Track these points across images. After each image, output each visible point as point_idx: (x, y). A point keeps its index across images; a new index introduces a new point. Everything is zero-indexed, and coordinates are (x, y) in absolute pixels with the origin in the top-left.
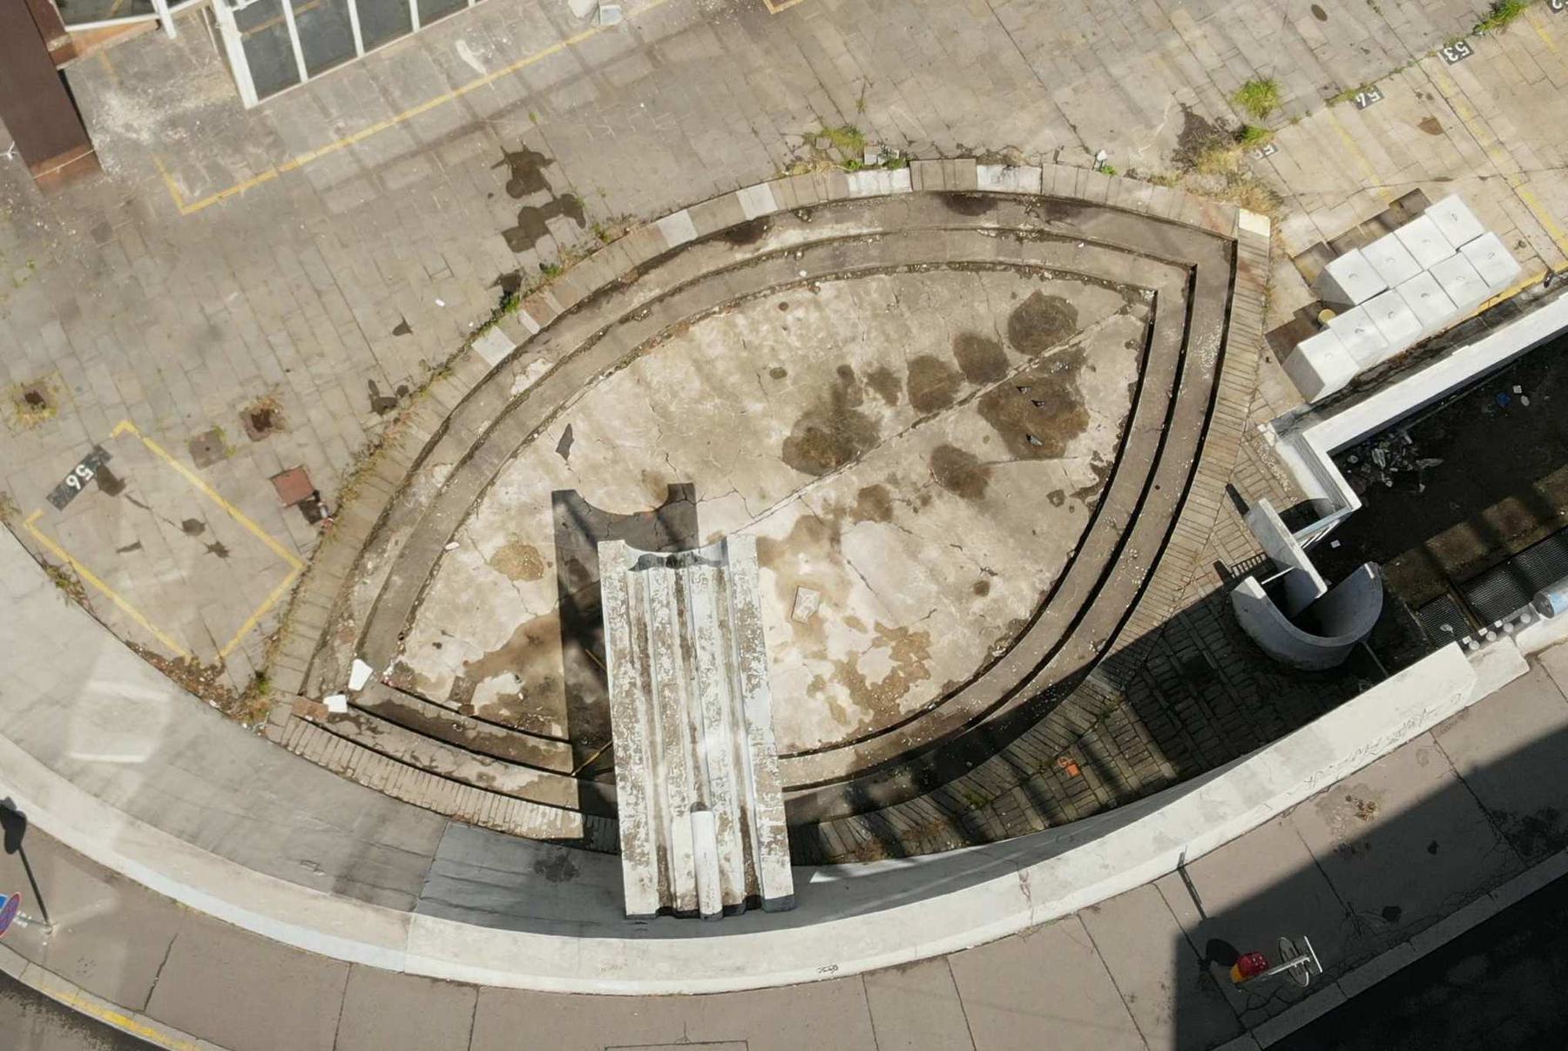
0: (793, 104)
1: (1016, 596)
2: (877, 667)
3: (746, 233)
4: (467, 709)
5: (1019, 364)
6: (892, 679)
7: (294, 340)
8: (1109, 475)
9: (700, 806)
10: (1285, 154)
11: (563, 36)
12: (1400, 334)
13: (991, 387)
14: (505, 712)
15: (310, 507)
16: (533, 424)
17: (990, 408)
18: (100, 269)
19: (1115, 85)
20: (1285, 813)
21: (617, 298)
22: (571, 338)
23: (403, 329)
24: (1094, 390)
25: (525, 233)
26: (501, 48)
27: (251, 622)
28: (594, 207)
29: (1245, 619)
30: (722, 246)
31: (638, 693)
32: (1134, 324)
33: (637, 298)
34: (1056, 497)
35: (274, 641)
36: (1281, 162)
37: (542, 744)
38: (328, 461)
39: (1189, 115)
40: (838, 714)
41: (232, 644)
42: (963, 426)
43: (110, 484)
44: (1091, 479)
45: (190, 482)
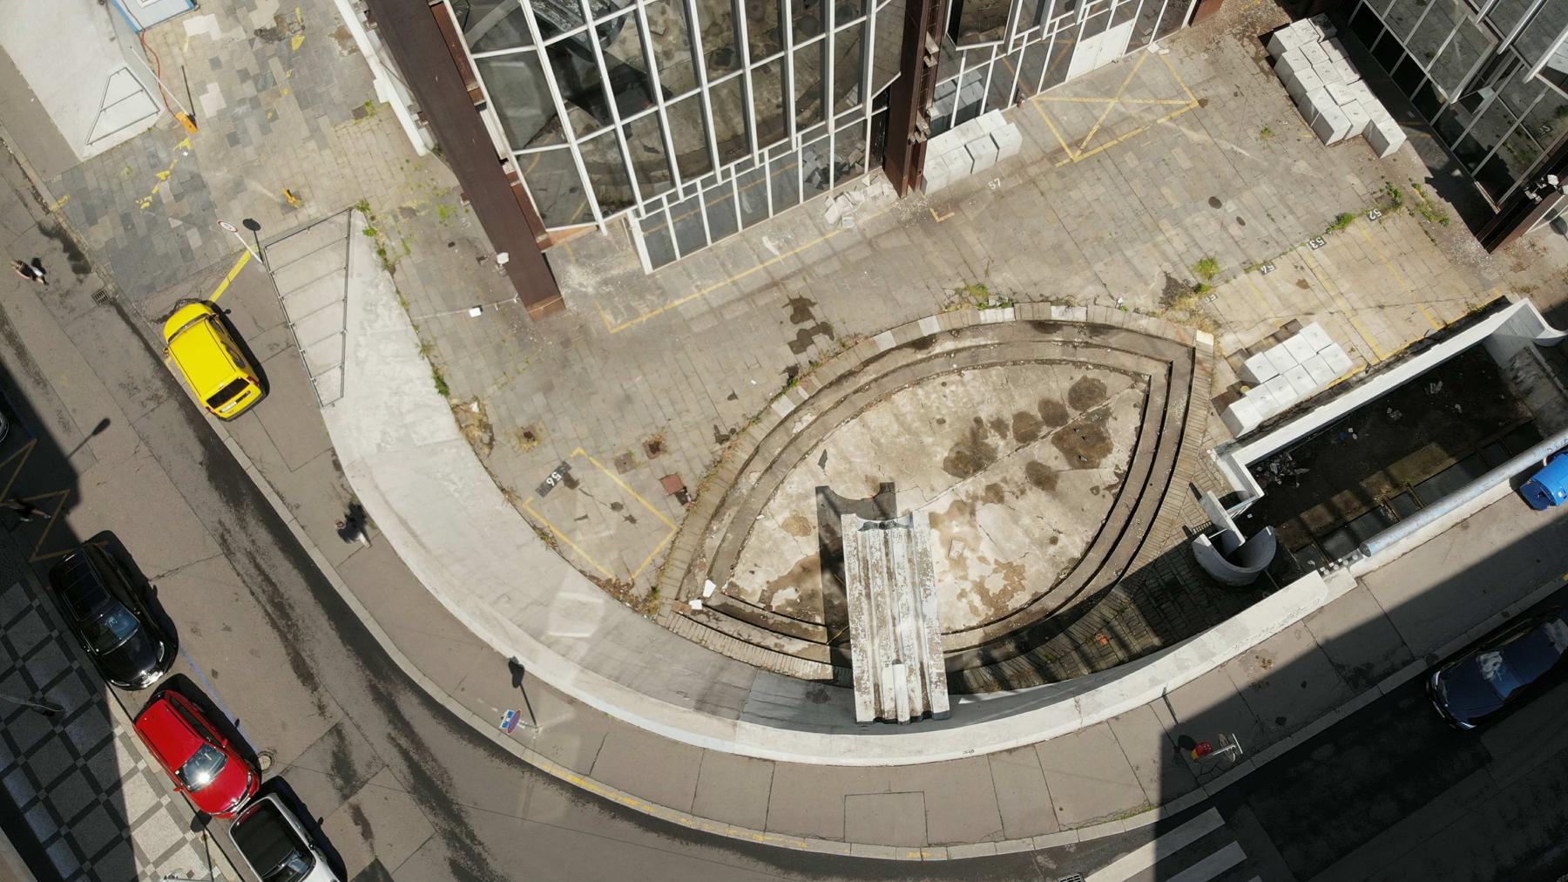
0: (949, 272)
1: (1073, 545)
2: (996, 584)
3: (923, 343)
4: (769, 607)
5: (1075, 416)
6: (1004, 591)
7: (673, 403)
8: (1124, 478)
9: (898, 662)
10: (1222, 299)
11: (822, 234)
12: (1285, 399)
13: (1059, 429)
14: (790, 609)
15: (682, 496)
16: (805, 449)
17: (1058, 440)
18: (565, 364)
19: (1128, 261)
20: (1222, 665)
21: (852, 379)
22: (826, 402)
23: (733, 397)
24: (1116, 431)
25: (800, 344)
26: (787, 241)
27: (649, 560)
28: (839, 329)
29: (1200, 558)
30: (910, 351)
31: (863, 599)
32: (1138, 394)
33: (863, 379)
34: (1095, 490)
35: (661, 570)
36: (1220, 304)
37: (810, 627)
38: (691, 470)
39: (1169, 278)
40: (974, 610)
41: (638, 572)
42: (1045, 452)
43: (571, 483)
44: (1114, 480)
45: (615, 482)
